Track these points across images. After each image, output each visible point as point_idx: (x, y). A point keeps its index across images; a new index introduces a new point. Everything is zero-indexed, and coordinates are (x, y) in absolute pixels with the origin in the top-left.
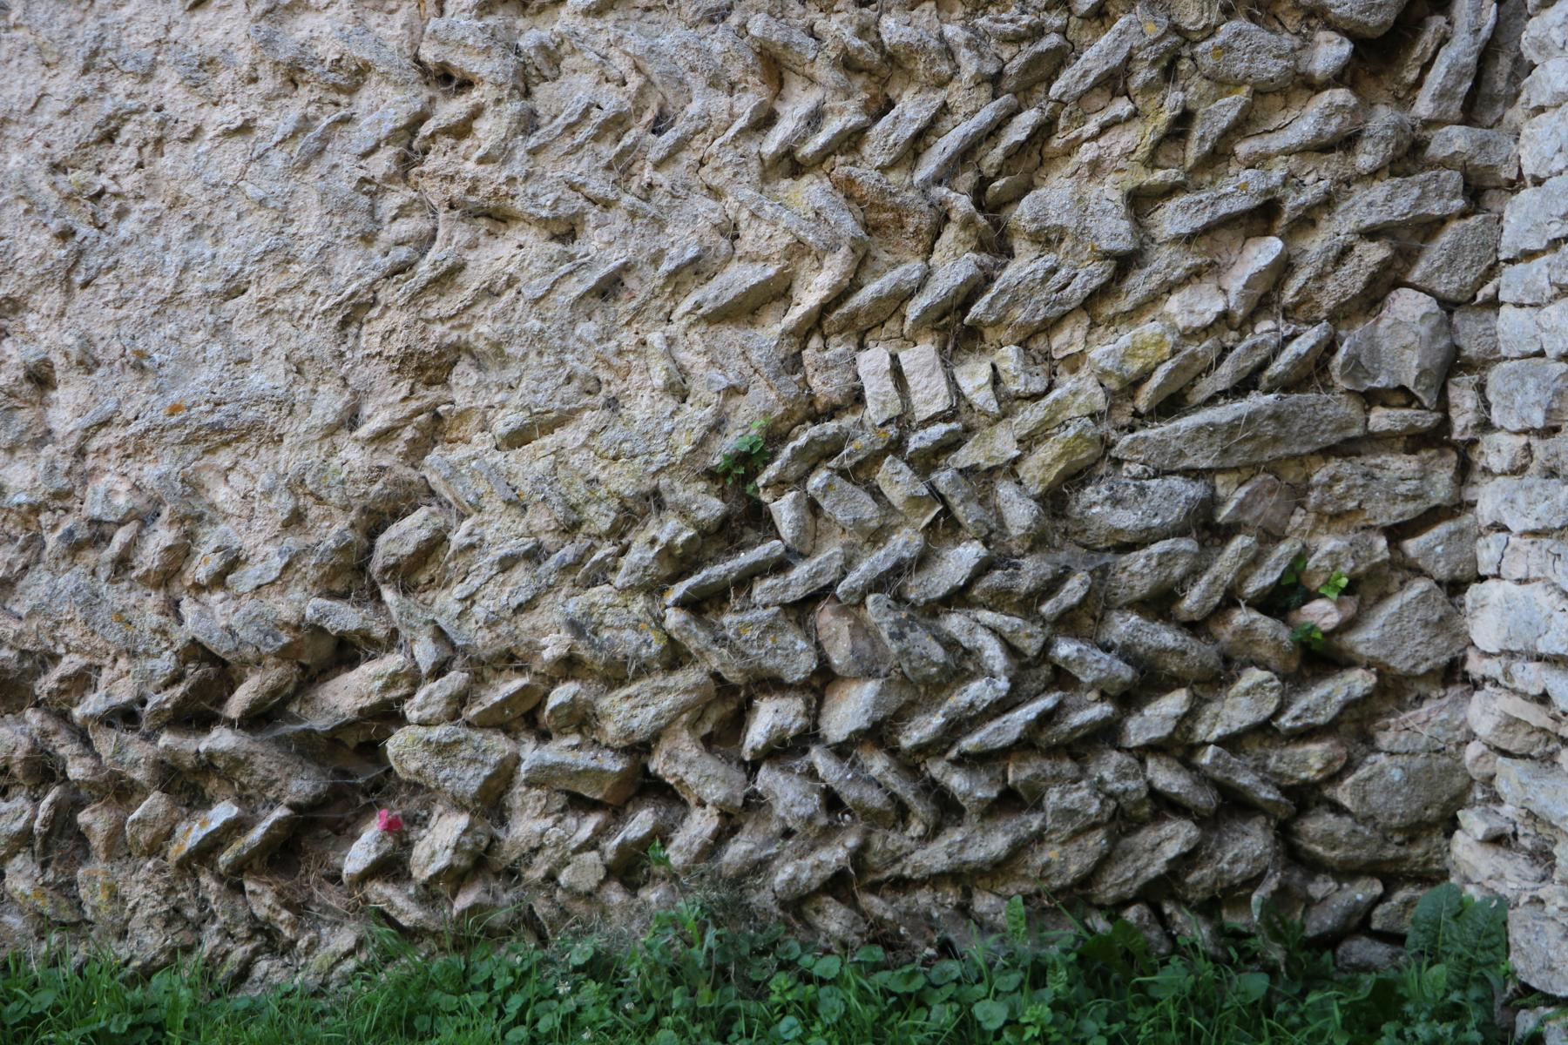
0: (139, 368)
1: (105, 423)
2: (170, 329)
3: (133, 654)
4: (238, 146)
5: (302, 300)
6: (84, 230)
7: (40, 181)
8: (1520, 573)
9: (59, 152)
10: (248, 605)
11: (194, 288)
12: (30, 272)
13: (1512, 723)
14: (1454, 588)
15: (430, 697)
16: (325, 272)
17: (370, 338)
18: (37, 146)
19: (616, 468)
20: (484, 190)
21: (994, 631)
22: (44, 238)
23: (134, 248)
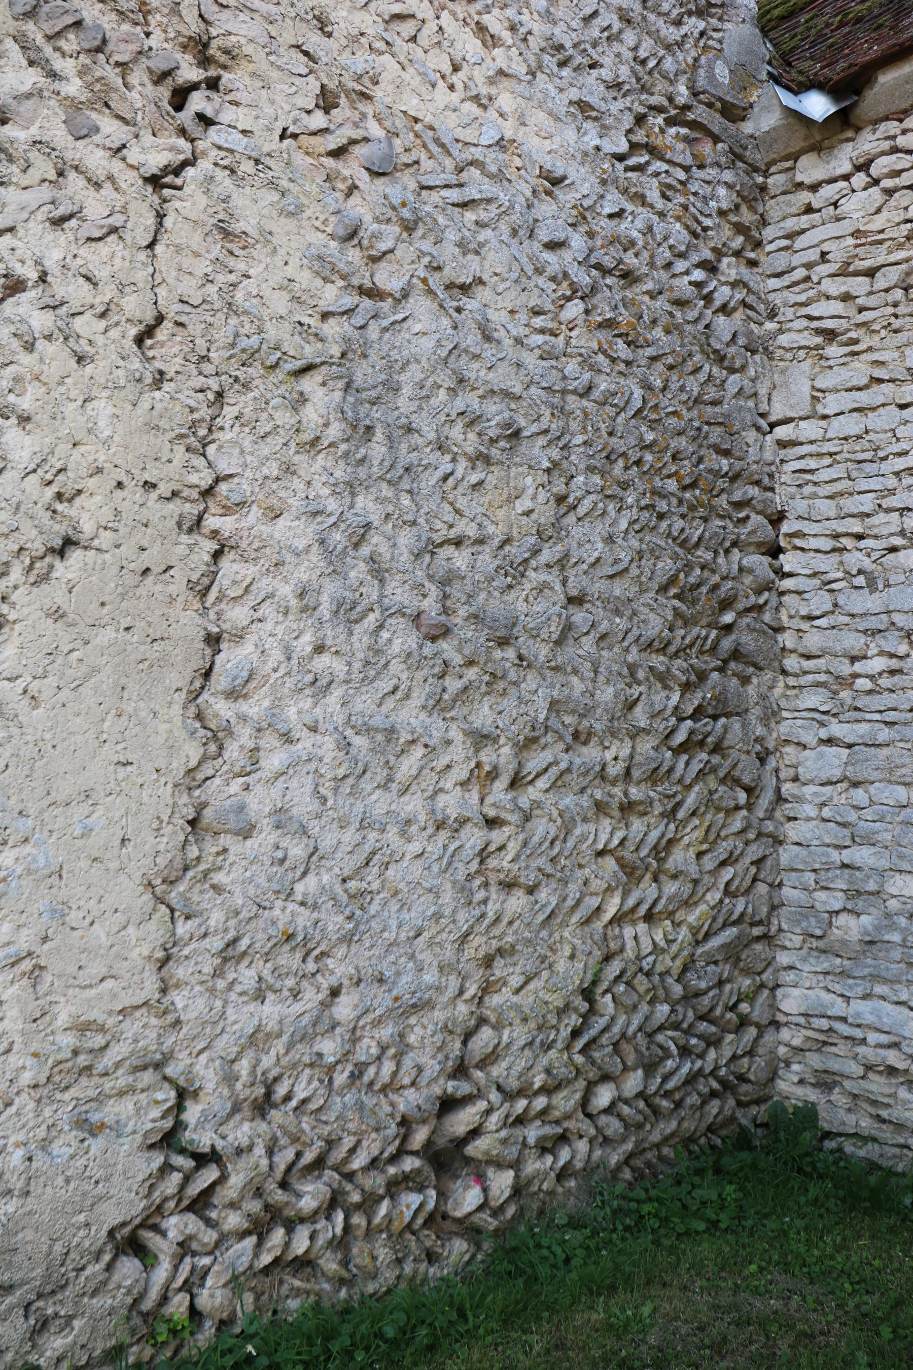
0: (381, 981)
1: (366, 1012)
2: (392, 958)
3: (377, 1130)
4: (419, 862)
5: (444, 935)
6: (358, 912)
7: (338, 889)
8: (808, 985)
9: (347, 872)
10: (425, 1092)
11: (403, 936)
12: (335, 937)
13: (808, 1038)
14: (773, 989)
15: (494, 1120)
16: (454, 921)
17: (469, 952)
18: (337, 870)
19: (555, 996)
20: (511, 875)
21: (672, 1038)
22: (340, 918)
23: (378, 920)
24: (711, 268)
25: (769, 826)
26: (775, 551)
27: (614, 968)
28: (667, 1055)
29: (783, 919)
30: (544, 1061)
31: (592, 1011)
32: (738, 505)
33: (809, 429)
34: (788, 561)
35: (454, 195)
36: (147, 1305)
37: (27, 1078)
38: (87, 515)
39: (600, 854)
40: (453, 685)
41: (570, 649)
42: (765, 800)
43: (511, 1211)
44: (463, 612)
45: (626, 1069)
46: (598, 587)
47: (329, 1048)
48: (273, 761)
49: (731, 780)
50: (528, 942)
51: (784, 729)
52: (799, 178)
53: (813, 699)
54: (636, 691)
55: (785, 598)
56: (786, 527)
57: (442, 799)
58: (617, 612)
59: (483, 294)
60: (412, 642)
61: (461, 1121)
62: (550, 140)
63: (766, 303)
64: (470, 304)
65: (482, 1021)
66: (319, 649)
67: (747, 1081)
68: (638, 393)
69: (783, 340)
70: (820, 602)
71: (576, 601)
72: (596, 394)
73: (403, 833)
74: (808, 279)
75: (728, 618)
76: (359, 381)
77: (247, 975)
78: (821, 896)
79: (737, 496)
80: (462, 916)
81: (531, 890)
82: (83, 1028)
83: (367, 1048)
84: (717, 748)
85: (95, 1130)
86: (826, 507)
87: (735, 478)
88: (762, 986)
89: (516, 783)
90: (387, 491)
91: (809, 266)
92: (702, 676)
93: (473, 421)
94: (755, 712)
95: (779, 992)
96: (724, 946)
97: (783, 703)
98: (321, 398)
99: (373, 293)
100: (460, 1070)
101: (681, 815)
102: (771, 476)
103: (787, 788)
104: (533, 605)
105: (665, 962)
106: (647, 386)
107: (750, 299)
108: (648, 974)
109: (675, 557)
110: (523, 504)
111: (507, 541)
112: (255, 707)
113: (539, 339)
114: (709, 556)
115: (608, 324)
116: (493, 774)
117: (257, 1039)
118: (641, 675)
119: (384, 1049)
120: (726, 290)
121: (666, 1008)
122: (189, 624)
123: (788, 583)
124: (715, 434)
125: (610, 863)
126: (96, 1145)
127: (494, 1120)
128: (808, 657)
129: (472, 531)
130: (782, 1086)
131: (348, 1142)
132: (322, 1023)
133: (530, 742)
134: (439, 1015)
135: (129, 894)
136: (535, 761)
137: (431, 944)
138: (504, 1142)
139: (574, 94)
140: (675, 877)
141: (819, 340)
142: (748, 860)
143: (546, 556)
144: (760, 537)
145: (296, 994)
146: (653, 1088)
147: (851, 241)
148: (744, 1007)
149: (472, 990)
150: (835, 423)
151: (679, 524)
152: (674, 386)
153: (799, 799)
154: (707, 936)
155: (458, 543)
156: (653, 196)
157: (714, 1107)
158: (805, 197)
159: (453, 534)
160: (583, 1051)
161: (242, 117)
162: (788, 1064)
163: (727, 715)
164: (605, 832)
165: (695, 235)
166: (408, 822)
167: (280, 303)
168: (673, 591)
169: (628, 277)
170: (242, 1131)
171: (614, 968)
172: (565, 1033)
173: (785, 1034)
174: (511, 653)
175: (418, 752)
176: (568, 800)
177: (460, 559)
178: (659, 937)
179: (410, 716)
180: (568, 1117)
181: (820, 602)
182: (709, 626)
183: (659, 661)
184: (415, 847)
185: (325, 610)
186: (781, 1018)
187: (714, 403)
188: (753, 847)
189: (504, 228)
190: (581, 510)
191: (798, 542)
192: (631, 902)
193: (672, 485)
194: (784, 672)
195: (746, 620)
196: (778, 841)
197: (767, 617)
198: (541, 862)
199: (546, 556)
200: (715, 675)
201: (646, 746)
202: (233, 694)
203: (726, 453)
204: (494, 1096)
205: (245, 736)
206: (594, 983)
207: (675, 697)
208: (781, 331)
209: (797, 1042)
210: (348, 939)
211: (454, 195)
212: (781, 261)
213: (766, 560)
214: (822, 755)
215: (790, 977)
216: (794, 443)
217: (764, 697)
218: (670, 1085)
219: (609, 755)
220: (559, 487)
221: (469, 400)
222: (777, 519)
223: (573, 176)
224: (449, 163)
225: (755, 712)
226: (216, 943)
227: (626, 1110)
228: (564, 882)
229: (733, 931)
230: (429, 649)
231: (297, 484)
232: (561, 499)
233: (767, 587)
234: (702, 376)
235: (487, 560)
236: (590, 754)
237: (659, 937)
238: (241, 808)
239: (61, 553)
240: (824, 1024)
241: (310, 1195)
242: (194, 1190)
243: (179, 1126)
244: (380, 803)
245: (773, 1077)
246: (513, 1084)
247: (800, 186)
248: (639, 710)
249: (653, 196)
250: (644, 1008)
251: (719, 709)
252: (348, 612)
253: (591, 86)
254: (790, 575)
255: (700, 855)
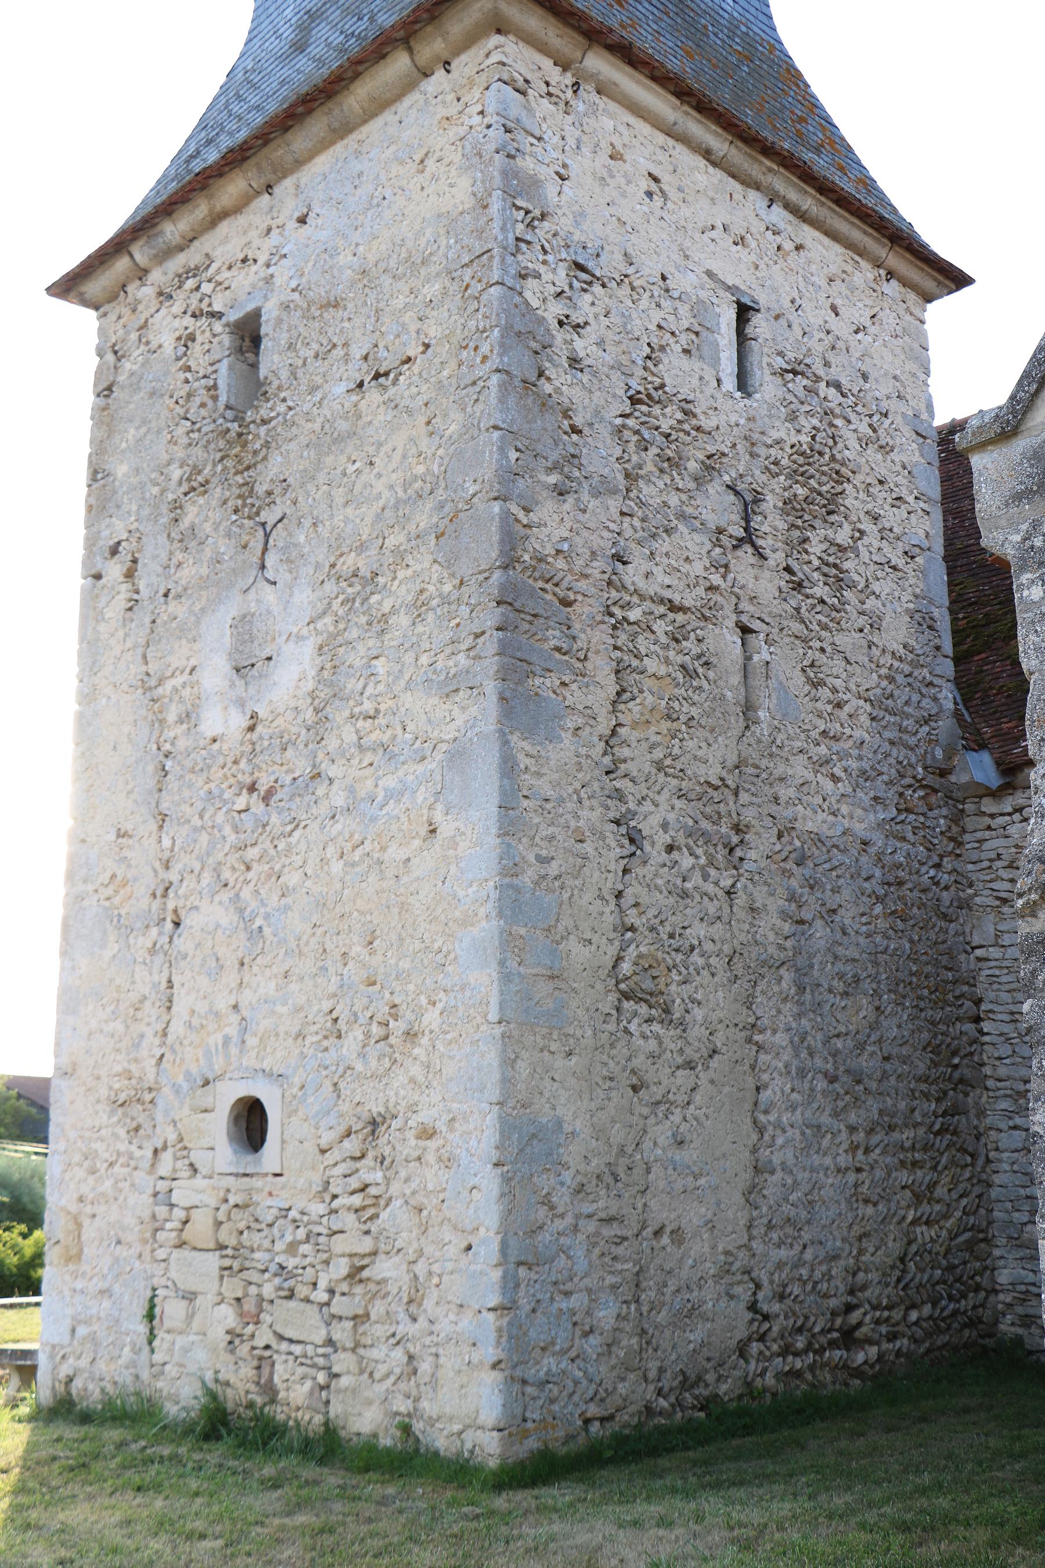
14: (994, 1269)
15: (868, 1318)
17: (853, 1233)
24: (938, 866)
25: (984, 1176)
26: (977, 1020)
27: (914, 1248)
28: (942, 1298)
29: (994, 1231)
30: (886, 1292)
31: (904, 1271)
32: (957, 998)
33: (994, 952)
34: (986, 1026)
35: (827, 866)
36: (749, 1379)
37: (712, 1272)
38: (719, 1041)
39: (903, 1188)
40: (841, 1104)
41: (885, 1083)
42: (981, 1161)
43: (877, 1367)
44: (842, 1069)
45: (923, 1303)
46: (895, 1051)
47: (804, 1272)
48: (780, 1141)
49: (963, 1150)
50: (876, 1230)
51: (988, 1121)
52: (983, 809)
53: (1004, 1104)
54: (915, 1103)
55: (985, 1047)
56: (983, 1007)
57: (839, 1159)
58: (904, 1063)
59: (842, 912)
60: (825, 1085)
61: (855, 1317)
62: (863, 822)
63: (967, 878)
64: (837, 919)
65: (859, 1269)
66: (793, 1090)
67: (982, 1322)
68: (908, 946)
69: (978, 900)
70: (1005, 1050)
71: (886, 1059)
72: (890, 951)
73: (825, 1174)
74: (990, 867)
75: (956, 1061)
76: (799, 964)
77: (775, 1236)
78: (1016, 1215)
79: (957, 993)
80: (849, 1215)
81: (875, 1204)
82: (727, 1253)
83: (817, 1275)
84: (955, 1133)
85: (732, 1297)
86: (1005, 997)
87: (955, 982)
88: (986, 1268)
89: (867, 1151)
90: (812, 1016)
91: (991, 860)
92: (945, 1093)
93: (841, 976)
94: (973, 1112)
95: (996, 1273)
96: (966, 1241)
97: (987, 1106)
98: (787, 976)
99: (801, 922)
100: (851, 1292)
101: (939, 1168)
102: (974, 978)
103: (992, 1155)
104: (868, 1062)
105: (937, 1248)
106: (911, 941)
107: (959, 879)
108: (930, 1252)
109: (929, 1031)
110: (862, 1014)
111: (858, 1032)
112: (772, 1117)
113: (864, 928)
114: (945, 1028)
115: (894, 912)
116: (857, 1147)
117: (780, 1265)
118: (917, 1094)
119: (823, 1275)
120: (946, 876)
121: (939, 1272)
122: (750, 1082)
123: (986, 1039)
124: (945, 960)
125: (908, 1192)
126: (733, 1303)
127: (868, 1318)
128: (1000, 1080)
129: (843, 1030)
130: (1002, 1327)
131: (812, 1319)
132: (799, 1263)
133: (872, 1130)
134: (842, 1263)
135: (738, 1198)
136: (875, 1139)
137: (839, 1227)
138: (873, 1330)
139: (872, 794)
140: (938, 1202)
141: (998, 903)
142: (973, 1195)
143: (873, 1038)
144: (970, 1014)
145: (791, 1245)
146: (936, 1315)
147: (1013, 850)
148: (978, 1278)
149: (855, 1252)
150: (1009, 950)
151: (930, 1013)
152: (924, 938)
153: (1000, 1161)
154: (956, 1236)
155: (838, 1036)
156: (910, 836)
157: (966, 1333)
158: (987, 820)
159: (836, 1032)
160: (903, 1289)
161: (752, 854)
162: (1004, 1315)
163: (959, 1114)
164: (903, 1177)
165: (930, 850)
166: (827, 1169)
167: (771, 936)
168: (929, 1049)
169: (900, 884)
170: (776, 1307)
171: (914, 1248)
172: (894, 1279)
173: (1001, 1297)
174: (861, 1087)
175: (829, 1136)
176: (888, 1160)
177: (839, 1044)
178: (933, 1234)
179: (825, 1119)
180: (898, 1324)
181: (1005, 1050)
182: (947, 1066)
183: (924, 1087)
184: (830, 1181)
185: (793, 1072)
186: (998, 1287)
187: (944, 942)
188: (977, 1188)
189: (848, 876)
190: (887, 1013)
191: (991, 1015)
192: (919, 1214)
193: (926, 992)
194: (987, 1089)
195: (965, 1061)
196: (989, 1185)
197: (976, 1058)
198: (879, 1190)
199: (873, 1038)
200: (951, 1092)
201: (921, 1131)
202: (766, 1112)
203: (950, 969)
204: (867, 1306)
205: (770, 1130)
206: (905, 1255)
207: (933, 1106)
208: (976, 895)
209: (1008, 1300)
210: (808, 1222)
211: (827, 866)
212: (975, 856)
213: (973, 1026)
214: (1011, 1136)
215: (1002, 1263)
216: (987, 960)
217: (977, 1104)
218: (945, 1314)
219: (904, 1137)
220: (877, 1003)
221: (840, 966)
222: (978, 1002)
223: (874, 838)
224: (824, 849)
225: (973, 1112)
226: (765, 1221)
227: (924, 1324)
228: (889, 1201)
229: (967, 1235)
230: (831, 1088)
231: (782, 1017)
232: (878, 1008)
233: (975, 1041)
234: (937, 929)
235: (850, 1043)
236: (896, 1135)
237: (933, 1234)
238: (771, 1161)
239: (710, 1056)
240: (1023, 1288)
241: (800, 1343)
242: (762, 1331)
243: (756, 1302)
244: (816, 1160)
245: (996, 1322)
246: (875, 1302)
247: (984, 814)
248: (917, 1113)
249: (910, 836)
250: (929, 1270)
251: (955, 1111)
252: (802, 1073)
253: (879, 786)
254: (987, 1034)
255: (950, 1190)
